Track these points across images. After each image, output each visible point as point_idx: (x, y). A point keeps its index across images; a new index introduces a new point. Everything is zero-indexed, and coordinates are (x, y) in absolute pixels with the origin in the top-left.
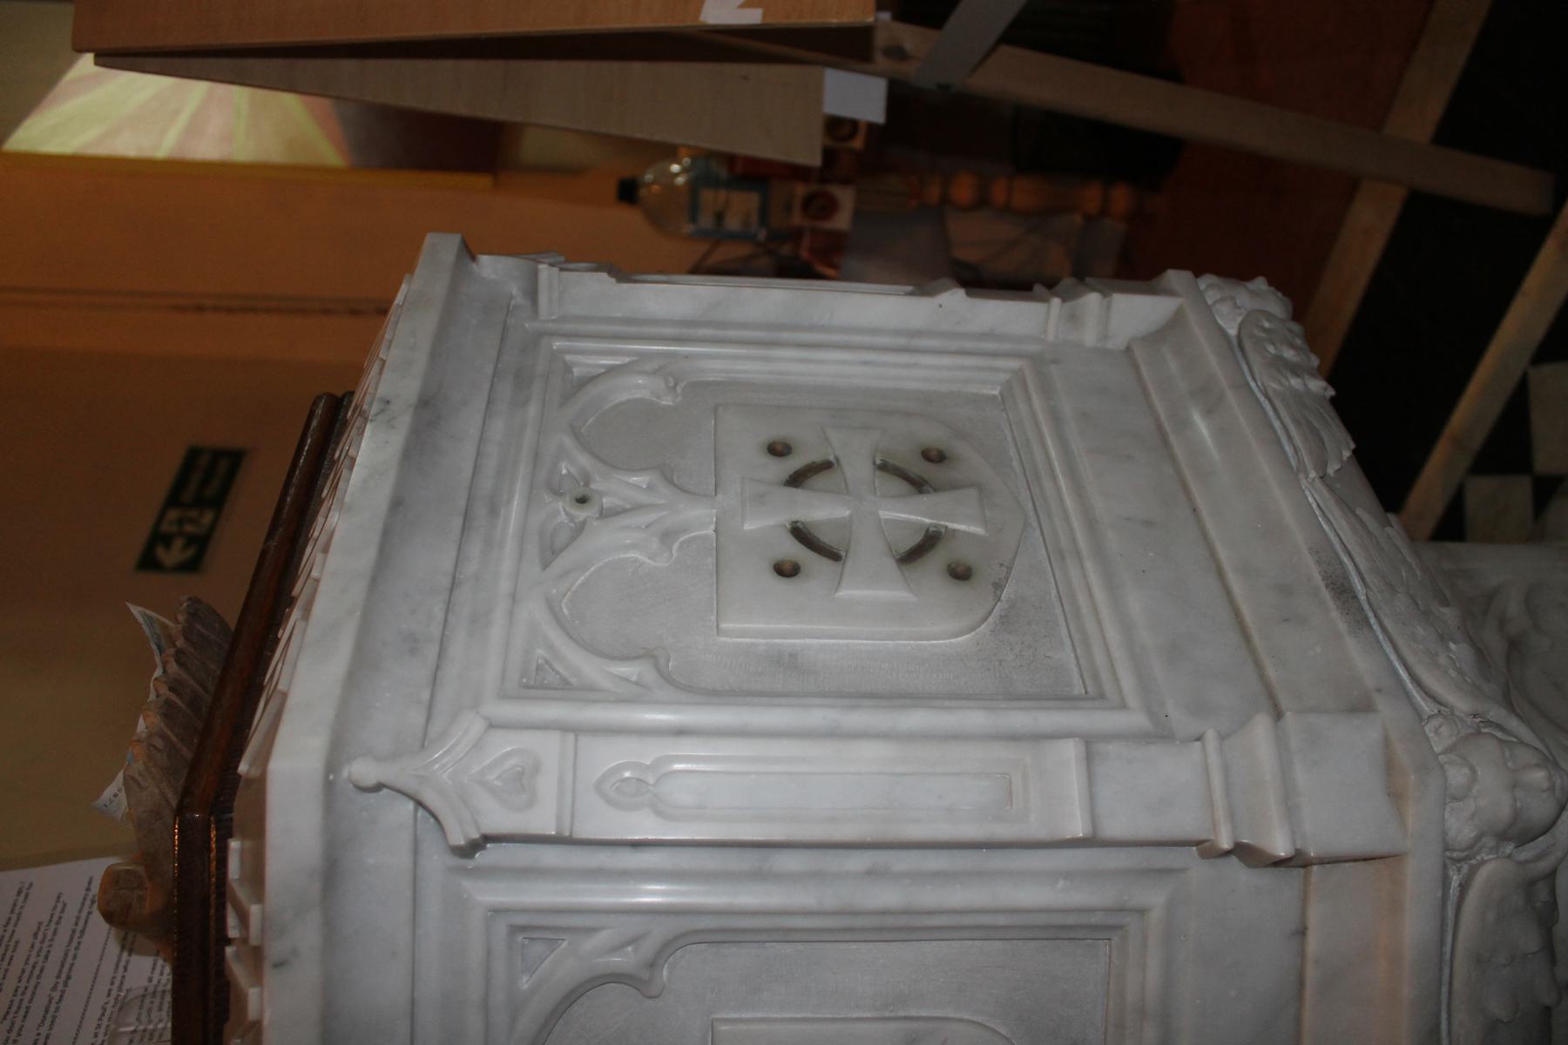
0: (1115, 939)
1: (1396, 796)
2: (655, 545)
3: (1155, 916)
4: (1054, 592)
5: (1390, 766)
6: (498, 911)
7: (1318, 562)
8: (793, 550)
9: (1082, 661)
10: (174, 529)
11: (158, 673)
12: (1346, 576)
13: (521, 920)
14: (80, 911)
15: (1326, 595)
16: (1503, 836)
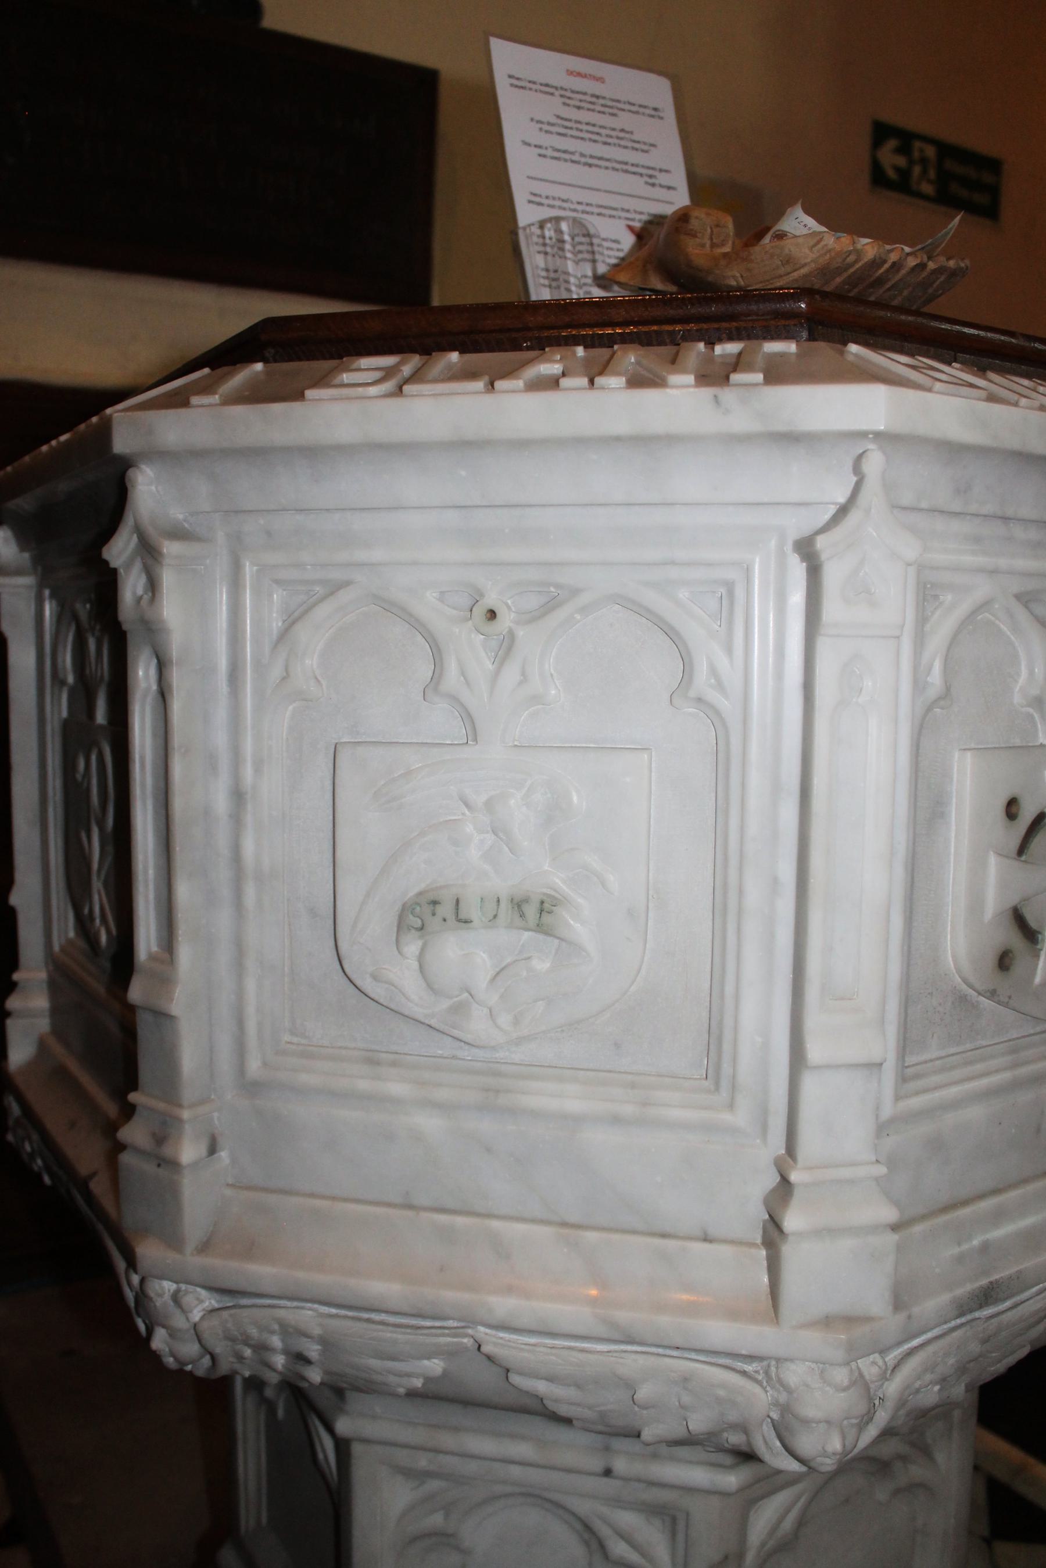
0: (706, 1083)
1: (827, 1322)
2: (1035, 691)
3: (727, 1117)
4: (984, 1043)
5: (850, 1320)
6: (748, 572)
7: (1010, 1277)
8: (1028, 813)
9: (929, 1065)
10: (916, 154)
11: (907, 249)
12: (997, 1301)
13: (740, 593)
14: (643, 167)
15: (984, 1282)
16: (785, 1409)
